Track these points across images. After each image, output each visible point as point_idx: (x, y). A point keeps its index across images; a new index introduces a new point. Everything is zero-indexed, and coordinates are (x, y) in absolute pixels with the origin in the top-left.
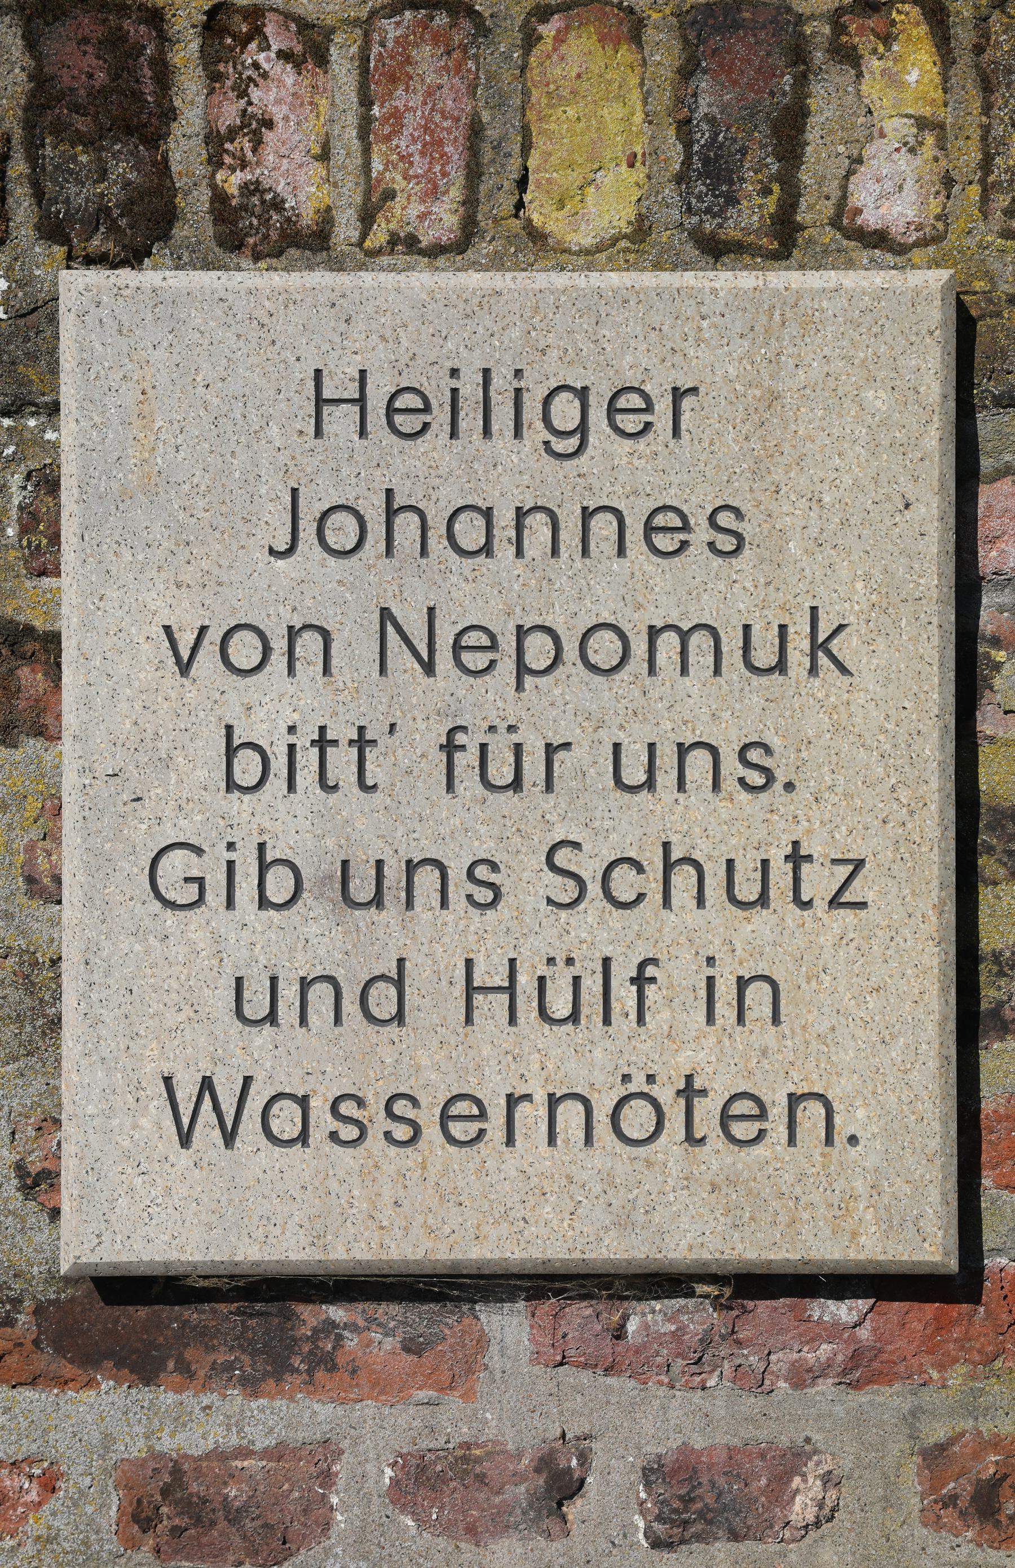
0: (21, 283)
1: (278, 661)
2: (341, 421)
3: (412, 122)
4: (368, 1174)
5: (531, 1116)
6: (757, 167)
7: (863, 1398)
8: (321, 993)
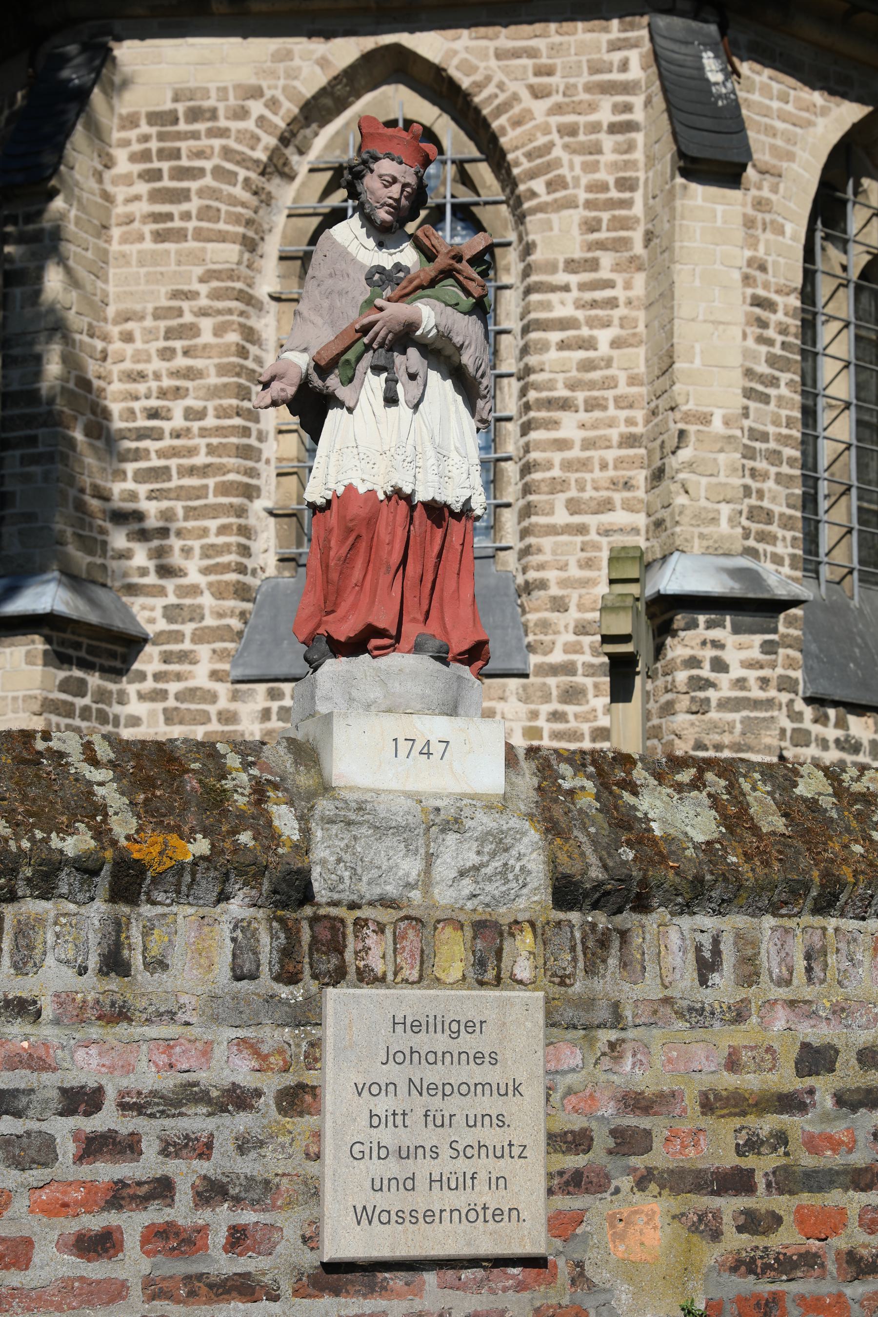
1: (383, 1092)
2: (399, 1028)
4: (405, 1231)
5: (446, 1215)
6: (491, 963)
8: (394, 1182)
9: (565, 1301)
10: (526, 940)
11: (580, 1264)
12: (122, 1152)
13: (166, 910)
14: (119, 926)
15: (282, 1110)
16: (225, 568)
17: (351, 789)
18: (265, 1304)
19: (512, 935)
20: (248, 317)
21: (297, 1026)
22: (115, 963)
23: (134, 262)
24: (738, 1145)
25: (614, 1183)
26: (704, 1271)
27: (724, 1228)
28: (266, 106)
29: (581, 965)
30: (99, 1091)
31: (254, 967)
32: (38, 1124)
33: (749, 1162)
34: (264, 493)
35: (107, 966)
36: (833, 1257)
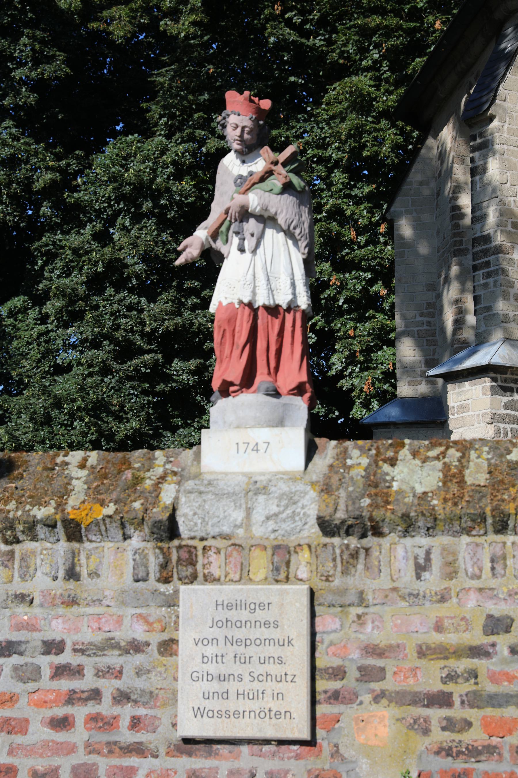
0: (175, 587)
2: (220, 608)
3: (233, 562)
5: (247, 714)
6: (283, 569)
7: (298, 762)
8: (216, 694)
9: (327, 767)
10: (305, 555)
11: (336, 746)
12: (74, 674)
13: (98, 545)
14: (74, 554)
15: (160, 653)
17: (211, 473)
18: (150, 759)
19: (296, 552)
21: (169, 606)
22: (72, 574)
25: (360, 698)
26: (418, 753)
27: (433, 728)
29: (339, 568)
30: (62, 643)
31: (144, 574)
33: (450, 687)
36: (508, 748)
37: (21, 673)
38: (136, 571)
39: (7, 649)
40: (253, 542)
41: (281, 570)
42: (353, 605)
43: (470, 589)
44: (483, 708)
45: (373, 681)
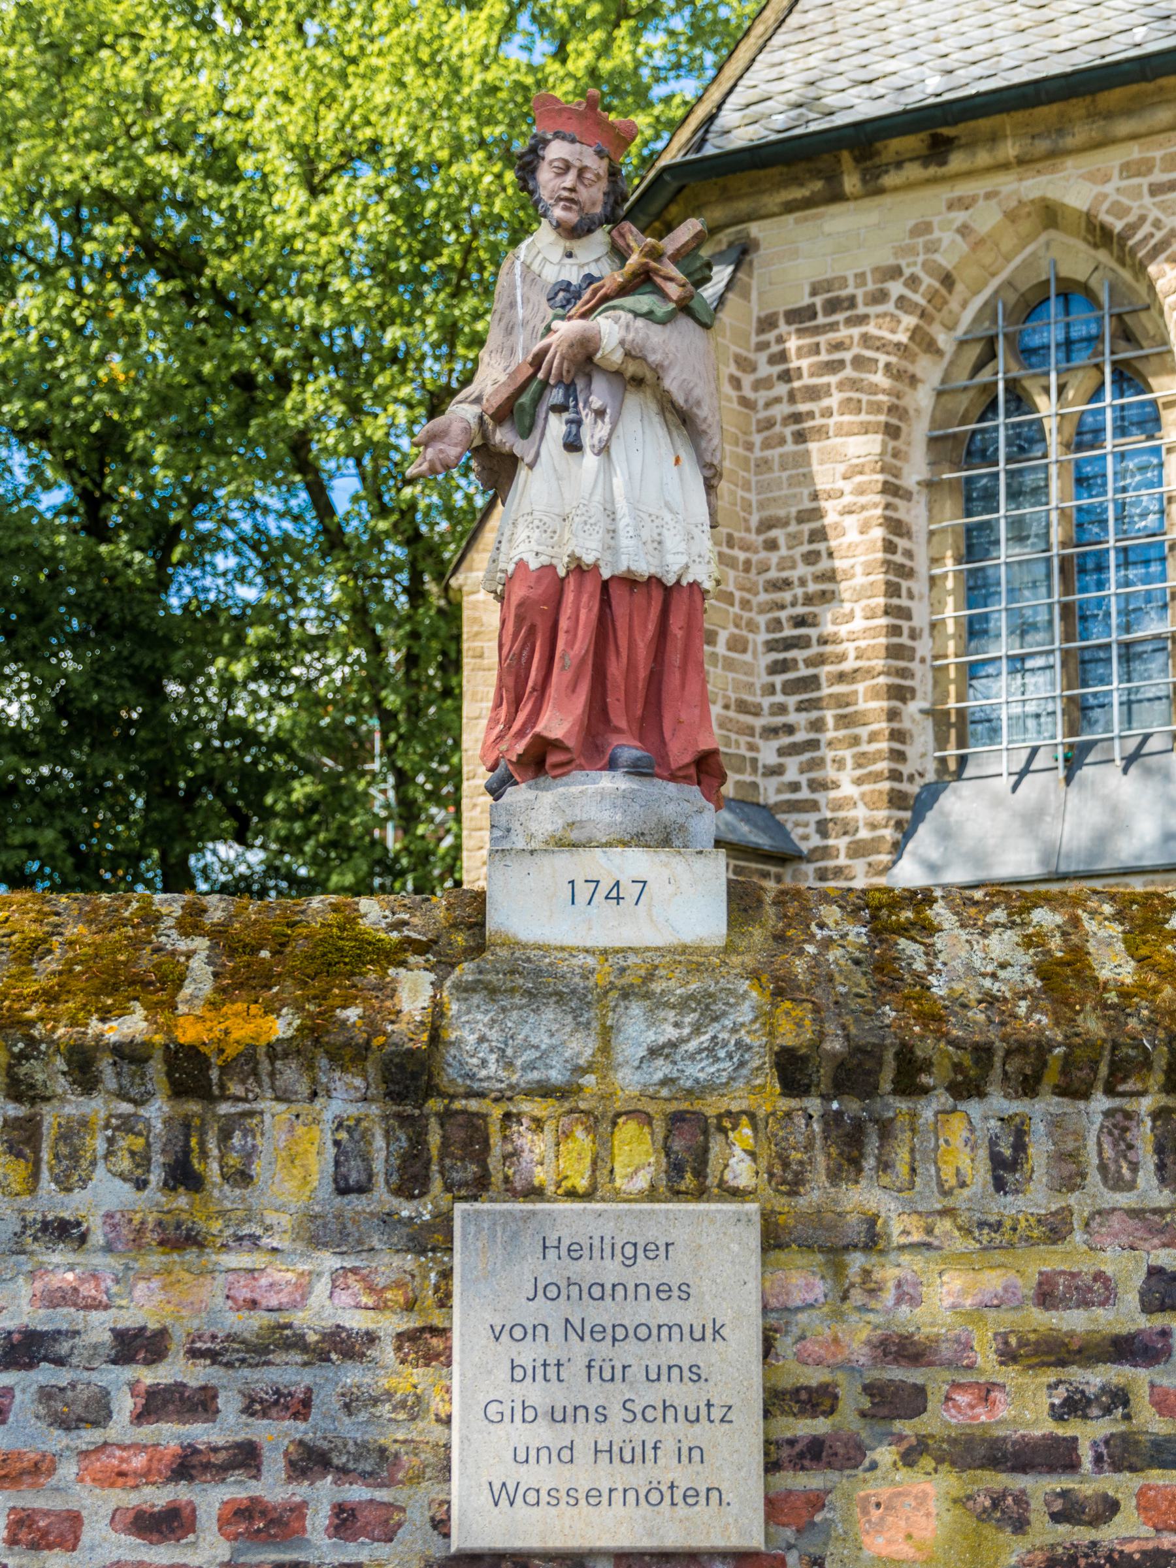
5: (617, 1496)
16: (876, 777)
20: (896, 509)
23: (776, 466)
24: (1052, 1405)
25: (871, 1456)
27: (1032, 1517)
28: (906, 284)
31: (364, 1177)
32: (86, 1374)
34: (919, 694)
35: (174, 1178)
37: (60, 1407)
38: (343, 1170)
39: (27, 1349)
40: (618, 1106)
41: (687, 1170)
42: (855, 1246)
43: (1114, 1210)
44: (1142, 1470)
45: (900, 1417)
